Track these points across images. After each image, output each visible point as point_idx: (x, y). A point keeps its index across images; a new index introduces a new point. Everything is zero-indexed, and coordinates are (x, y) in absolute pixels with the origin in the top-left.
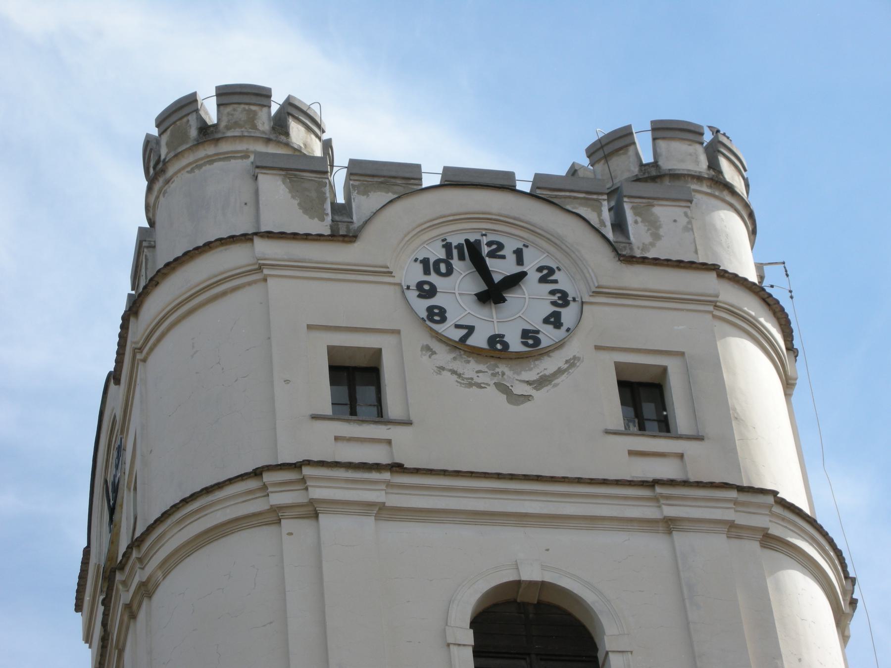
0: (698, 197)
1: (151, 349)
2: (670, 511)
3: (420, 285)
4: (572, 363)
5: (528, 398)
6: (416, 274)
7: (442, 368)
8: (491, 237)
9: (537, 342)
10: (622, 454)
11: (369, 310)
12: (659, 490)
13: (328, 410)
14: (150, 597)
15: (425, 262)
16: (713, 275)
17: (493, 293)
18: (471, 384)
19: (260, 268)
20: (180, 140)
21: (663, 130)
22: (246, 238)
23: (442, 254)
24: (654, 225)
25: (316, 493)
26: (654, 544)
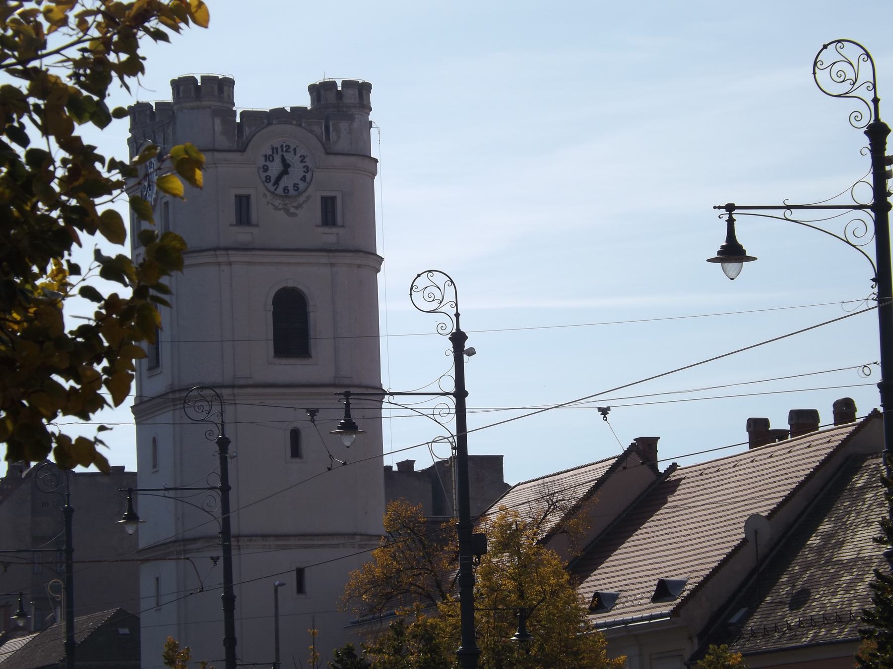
2: (332, 261)
3: (264, 166)
4: (308, 198)
13: (234, 223)
15: (265, 156)
25: (232, 259)
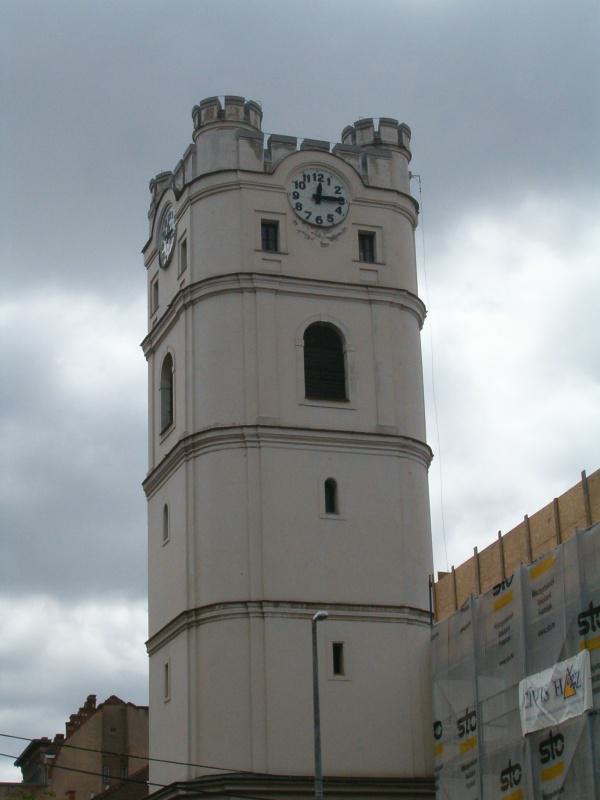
0: (393, 153)
6: (292, 188)
7: (299, 231)
8: (320, 172)
10: (356, 272)
11: (276, 204)
12: (370, 289)
13: (260, 248)
15: (296, 183)
16: (395, 195)
17: (318, 198)
19: (239, 184)
20: (211, 115)
21: (384, 122)
22: (235, 171)
23: (302, 179)
24: (376, 166)
26: (365, 308)
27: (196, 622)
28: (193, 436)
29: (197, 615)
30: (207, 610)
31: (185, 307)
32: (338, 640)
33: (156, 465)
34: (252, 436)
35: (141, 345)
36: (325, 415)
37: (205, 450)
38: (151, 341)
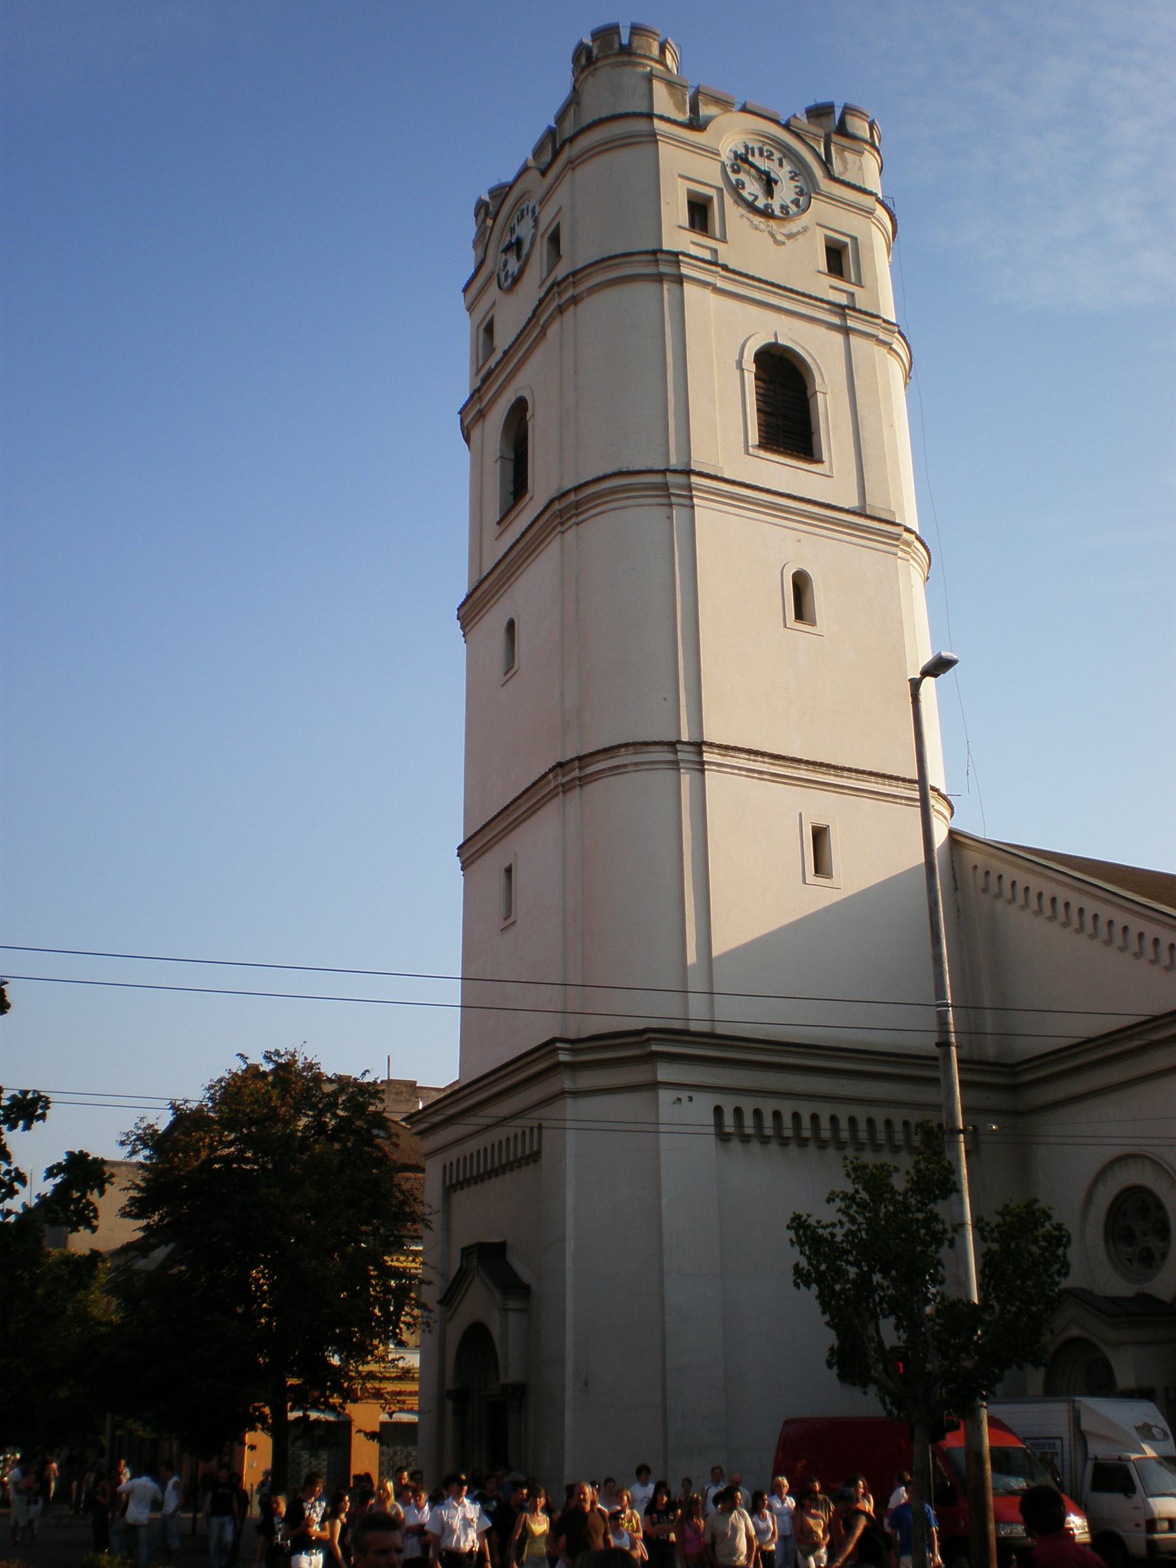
1: (579, 164)
4: (805, 229)
5: (784, 243)
9: (788, 213)
10: (826, 287)
14: (575, 304)
18: (756, 228)
24: (845, 162)
27: (580, 779)
28: (577, 489)
29: (581, 768)
30: (602, 756)
31: (561, 310)
32: (822, 822)
33: (485, 574)
34: (681, 487)
35: (460, 413)
36: (781, 472)
37: (599, 509)
38: (480, 399)
